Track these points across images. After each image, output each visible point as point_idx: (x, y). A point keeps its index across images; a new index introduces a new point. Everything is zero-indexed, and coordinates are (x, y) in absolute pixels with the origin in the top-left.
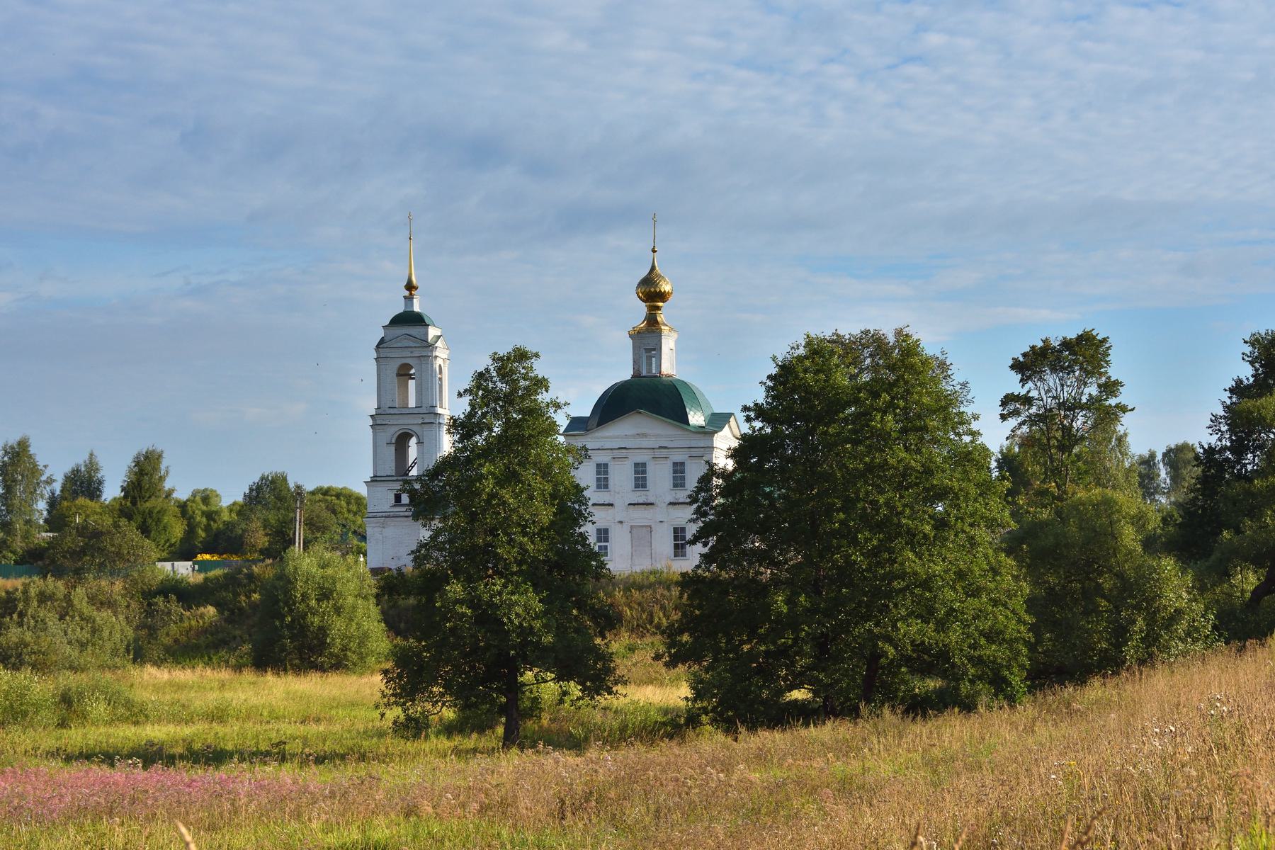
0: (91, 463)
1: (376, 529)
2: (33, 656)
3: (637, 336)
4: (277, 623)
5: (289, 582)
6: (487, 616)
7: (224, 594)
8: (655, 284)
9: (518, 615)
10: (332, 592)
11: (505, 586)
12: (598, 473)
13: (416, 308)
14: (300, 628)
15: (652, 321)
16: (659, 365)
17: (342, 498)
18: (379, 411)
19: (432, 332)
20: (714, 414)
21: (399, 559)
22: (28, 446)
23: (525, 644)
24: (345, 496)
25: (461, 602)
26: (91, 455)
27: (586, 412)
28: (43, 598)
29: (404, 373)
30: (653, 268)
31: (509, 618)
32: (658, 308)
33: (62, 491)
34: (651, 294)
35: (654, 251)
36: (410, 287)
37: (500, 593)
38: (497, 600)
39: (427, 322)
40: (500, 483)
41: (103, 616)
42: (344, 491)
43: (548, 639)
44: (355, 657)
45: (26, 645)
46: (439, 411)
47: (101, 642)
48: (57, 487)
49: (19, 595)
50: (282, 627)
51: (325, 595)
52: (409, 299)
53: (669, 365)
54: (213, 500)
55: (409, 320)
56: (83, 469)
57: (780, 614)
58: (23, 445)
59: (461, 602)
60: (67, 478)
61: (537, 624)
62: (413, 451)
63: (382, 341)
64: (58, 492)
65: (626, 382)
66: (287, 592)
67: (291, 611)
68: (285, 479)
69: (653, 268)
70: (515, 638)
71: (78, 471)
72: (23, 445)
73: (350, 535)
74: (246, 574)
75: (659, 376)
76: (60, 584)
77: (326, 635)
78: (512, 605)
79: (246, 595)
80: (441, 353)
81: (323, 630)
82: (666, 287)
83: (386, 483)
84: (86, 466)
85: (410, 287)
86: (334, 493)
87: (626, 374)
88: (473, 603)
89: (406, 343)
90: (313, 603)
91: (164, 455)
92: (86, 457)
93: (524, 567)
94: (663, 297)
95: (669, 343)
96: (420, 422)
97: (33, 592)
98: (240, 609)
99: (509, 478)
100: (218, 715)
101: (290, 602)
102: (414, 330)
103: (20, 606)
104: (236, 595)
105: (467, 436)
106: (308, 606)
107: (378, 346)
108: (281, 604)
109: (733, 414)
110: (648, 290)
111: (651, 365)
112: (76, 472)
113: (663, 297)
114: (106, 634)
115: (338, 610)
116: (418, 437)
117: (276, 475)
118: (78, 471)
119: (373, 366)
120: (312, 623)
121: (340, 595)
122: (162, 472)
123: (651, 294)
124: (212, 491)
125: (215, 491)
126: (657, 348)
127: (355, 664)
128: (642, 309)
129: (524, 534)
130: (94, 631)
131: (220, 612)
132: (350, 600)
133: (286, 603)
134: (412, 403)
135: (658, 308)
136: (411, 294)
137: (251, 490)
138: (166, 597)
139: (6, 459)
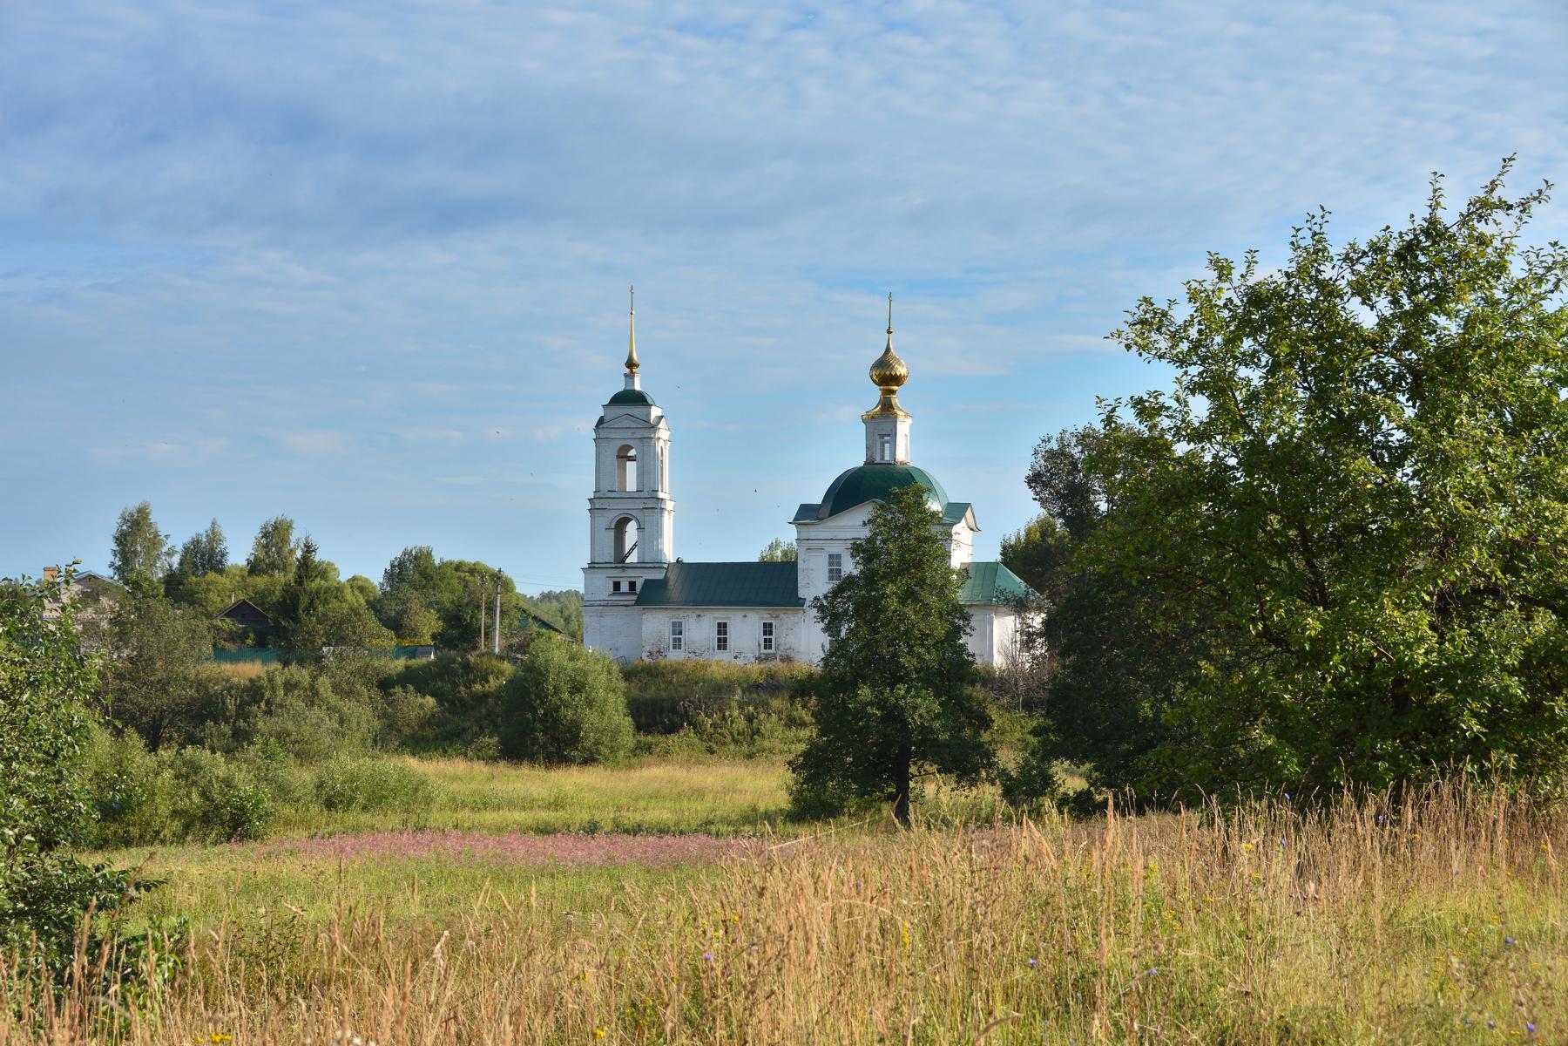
0: (213, 533)
1: (593, 618)
2: (296, 745)
3: (869, 420)
4: (529, 716)
5: (540, 673)
6: (894, 716)
7: (440, 683)
8: (890, 367)
9: (920, 715)
10: (584, 685)
11: (908, 691)
12: (831, 564)
13: (637, 387)
14: (552, 722)
15: (887, 407)
16: (893, 452)
17: (476, 574)
18: (598, 495)
19: (655, 412)
20: (949, 504)
21: (617, 650)
22: (148, 514)
23: (924, 741)
24: (480, 572)
25: (871, 704)
26: (214, 524)
27: (817, 499)
28: (290, 686)
29: (623, 456)
30: (888, 350)
31: (913, 718)
32: (893, 392)
33: (181, 564)
34: (886, 377)
35: (889, 332)
36: (631, 364)
37: (904, 697)
38: (902, 703)
39: (650, 401)
40: (903, 602)
41: (347, 706)
42: (478, 567)
43: (944, 737)
44: (607, 751)
45: (289, 735)
46: (661, 495)
47: (350, 732)
48: (176, 560)
49: (265, 682)
50: (534, 719)
51: (577, 688)
52: (630, 377)
53: (905, 450)
54: (331, 575)
55: (630, 399)
56: (204, 540)
57: (1146, 718)
58: (143, 512)
59: (871, 704)
60: (186, 549)
61: (937, 724)
62: (631, 534)
63: (601, 421)
64: (176, 566)
65: (860, 469)
66: (538, 684)
67: (543, 703)
68: (429, 554)
69: (888, 350)
70: (916, 737)
71: (198, 542)
72: (143, 512)
73: (530, 620)
74: (460, 664)
75: (892, 464)
76: (304, 672)
77: (579, 728)
78: (915, 708)
79: (465, 686)
80: (663, 433)
81: (576, 726)
82: (901, 370)
83: (605, 570)
84: (208, 536)
85: (631, 364)
86: (467, 569)
87: (857, 460)
88: (881, 705)
89: (627, 424)
90: (566, 696)
91: (294, 526)
92: (208, 526)
93: (922, 674)
94: (897, 380)
95: (903, 428)
96: (642, 506)
97: (279, 680)
98: (461, 700)
99: (909, 596)
100: (557, 804)
101: (542, 695)
102: (636, 410)
103: (267, 695)
104: (456, 685)
105: (868, 560)
106: (560, 698)
107: (597, 426)
108: (533, 697)
109: (967, 505)
110: (882, 373)
111: (883, 451)
112: (196, 542)
113: (897, 380)
114: (354, 725)
115: (590, 703)
116: (638, 522)
117: (421, 551)
118: (198, 542)
119: (591, 449)
120: (565, 716)
121: (592, 688)
122: (292, 545)
123: (886, 377)
124: (329, 564)
125: (333, 564)
126: (893, 434)
127: (607, 759)
128: (876, 393)
129: (923, 645)
130: (342, 722)
131: (440, 702)
132: (602, 693)
133: (538, 695)
134: (631, 485)
135: (893, 392)
136: (632, 372)
137: (393, 566)
138: (404, 687)
139: (125, 527)
